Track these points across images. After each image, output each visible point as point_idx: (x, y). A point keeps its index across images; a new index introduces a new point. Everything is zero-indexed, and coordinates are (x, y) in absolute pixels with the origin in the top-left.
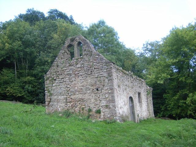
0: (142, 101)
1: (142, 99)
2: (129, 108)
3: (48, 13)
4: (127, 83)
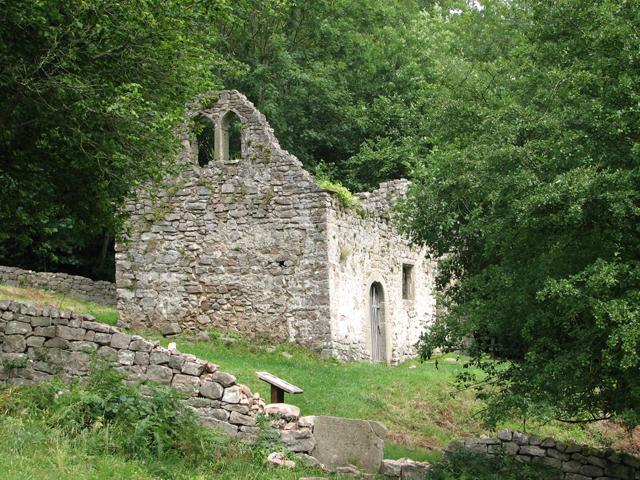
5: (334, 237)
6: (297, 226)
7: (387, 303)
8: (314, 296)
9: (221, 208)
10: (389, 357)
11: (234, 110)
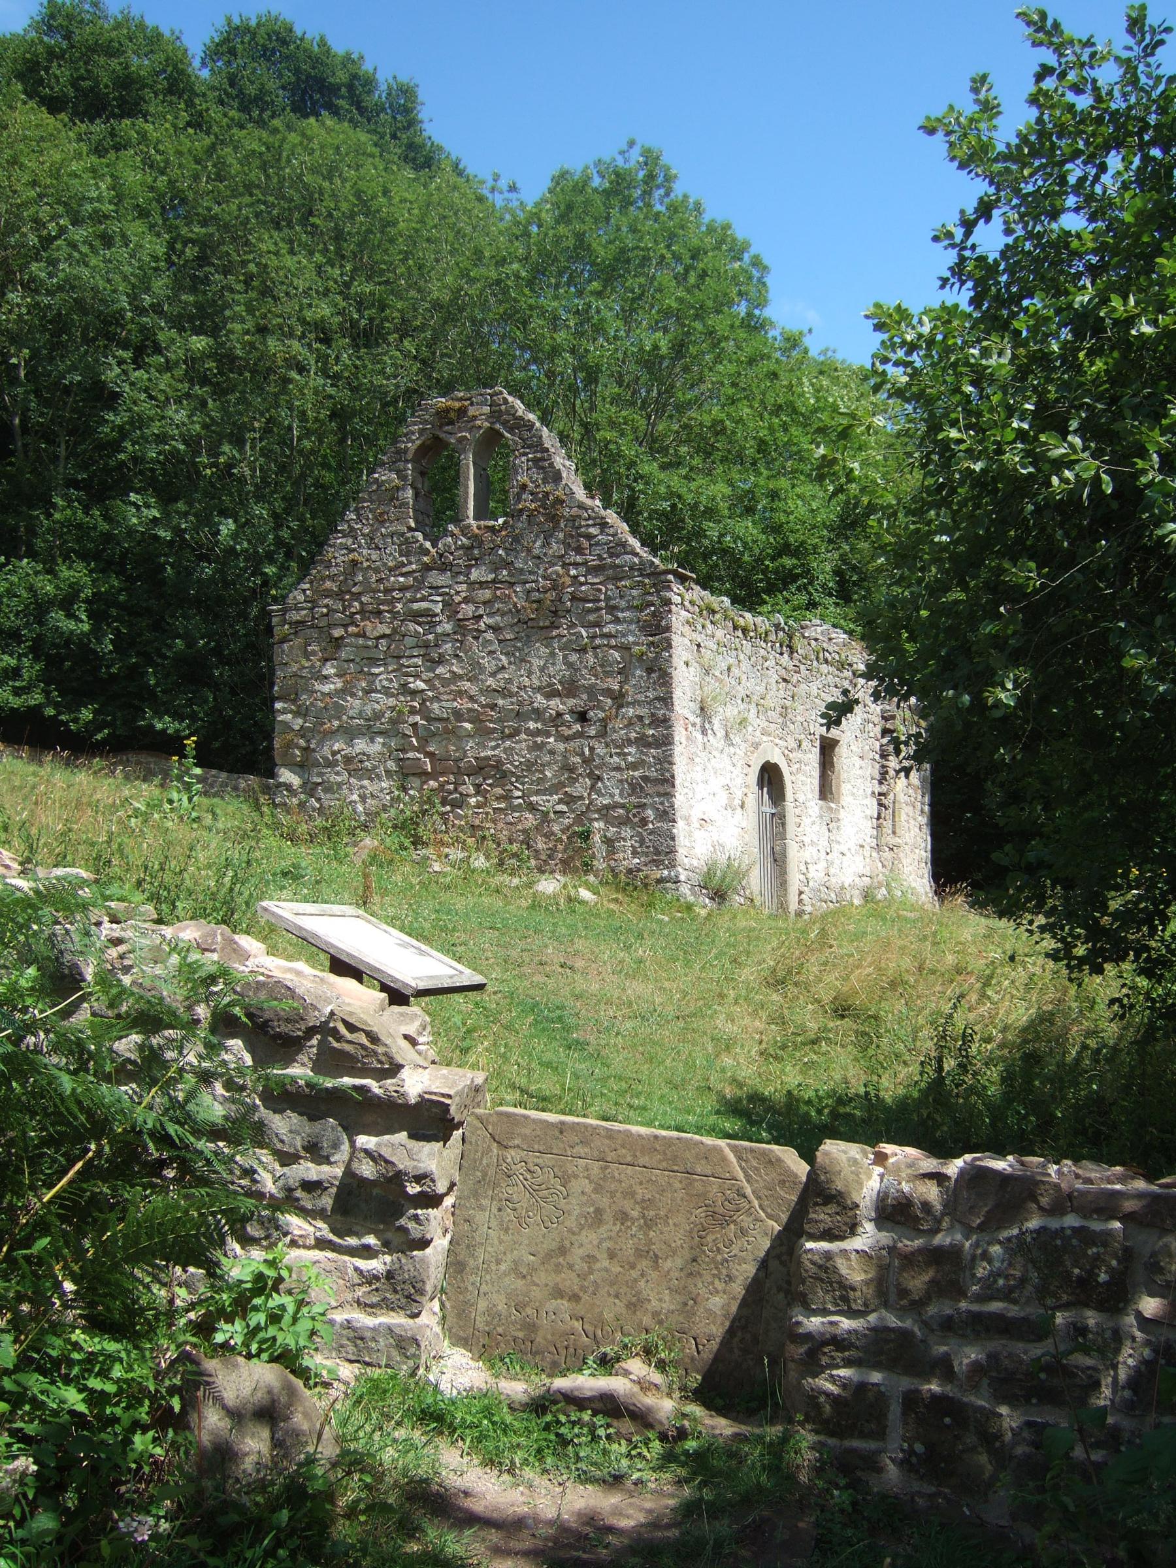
0: (845, 788)
1: (844, 776)
2: (839, 786)
3: (322, 39)
4: (752, 685)
5: (687, 664)
6: (613, 642)
7: (789, 805)
8: (645, 779)
9: (468, 610)
10: (793, 906)
11: (498, 426)
